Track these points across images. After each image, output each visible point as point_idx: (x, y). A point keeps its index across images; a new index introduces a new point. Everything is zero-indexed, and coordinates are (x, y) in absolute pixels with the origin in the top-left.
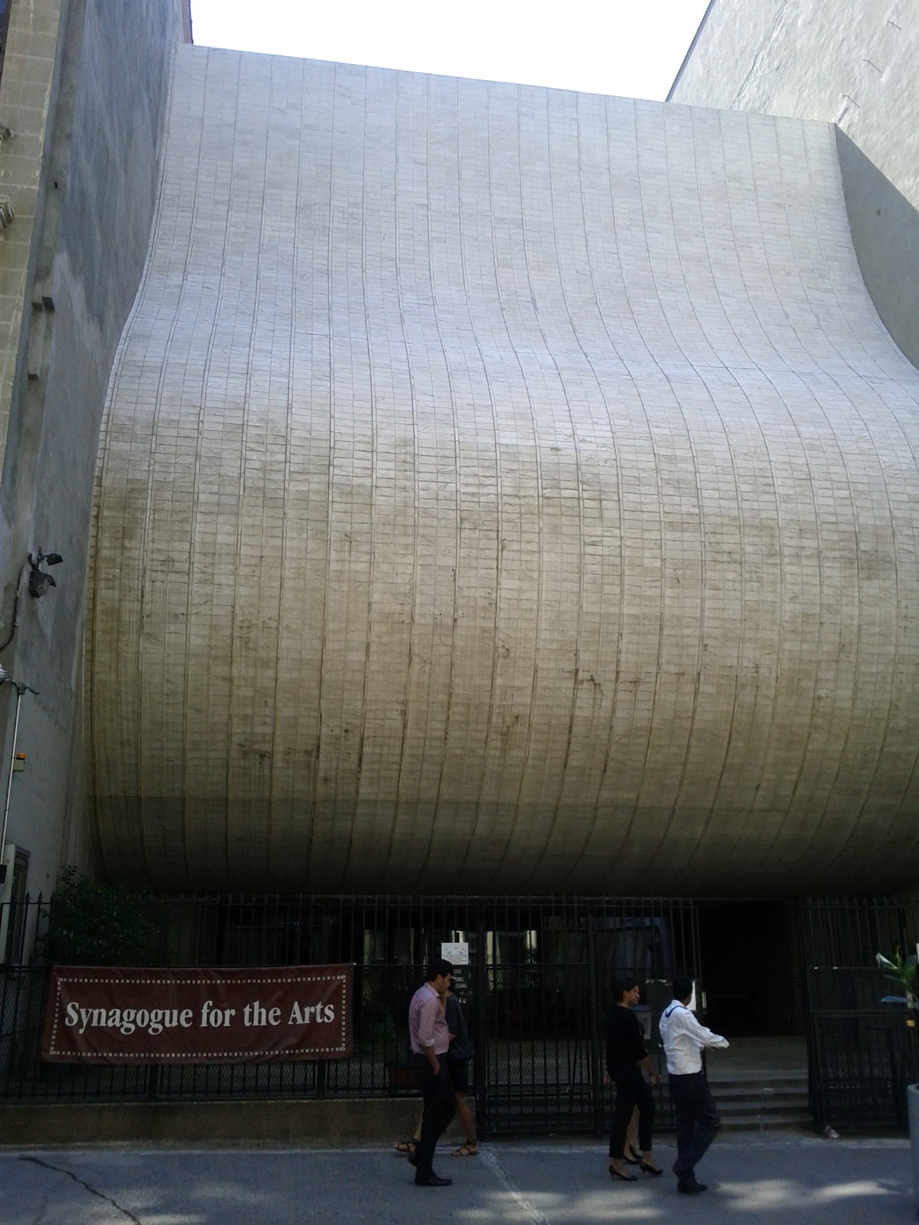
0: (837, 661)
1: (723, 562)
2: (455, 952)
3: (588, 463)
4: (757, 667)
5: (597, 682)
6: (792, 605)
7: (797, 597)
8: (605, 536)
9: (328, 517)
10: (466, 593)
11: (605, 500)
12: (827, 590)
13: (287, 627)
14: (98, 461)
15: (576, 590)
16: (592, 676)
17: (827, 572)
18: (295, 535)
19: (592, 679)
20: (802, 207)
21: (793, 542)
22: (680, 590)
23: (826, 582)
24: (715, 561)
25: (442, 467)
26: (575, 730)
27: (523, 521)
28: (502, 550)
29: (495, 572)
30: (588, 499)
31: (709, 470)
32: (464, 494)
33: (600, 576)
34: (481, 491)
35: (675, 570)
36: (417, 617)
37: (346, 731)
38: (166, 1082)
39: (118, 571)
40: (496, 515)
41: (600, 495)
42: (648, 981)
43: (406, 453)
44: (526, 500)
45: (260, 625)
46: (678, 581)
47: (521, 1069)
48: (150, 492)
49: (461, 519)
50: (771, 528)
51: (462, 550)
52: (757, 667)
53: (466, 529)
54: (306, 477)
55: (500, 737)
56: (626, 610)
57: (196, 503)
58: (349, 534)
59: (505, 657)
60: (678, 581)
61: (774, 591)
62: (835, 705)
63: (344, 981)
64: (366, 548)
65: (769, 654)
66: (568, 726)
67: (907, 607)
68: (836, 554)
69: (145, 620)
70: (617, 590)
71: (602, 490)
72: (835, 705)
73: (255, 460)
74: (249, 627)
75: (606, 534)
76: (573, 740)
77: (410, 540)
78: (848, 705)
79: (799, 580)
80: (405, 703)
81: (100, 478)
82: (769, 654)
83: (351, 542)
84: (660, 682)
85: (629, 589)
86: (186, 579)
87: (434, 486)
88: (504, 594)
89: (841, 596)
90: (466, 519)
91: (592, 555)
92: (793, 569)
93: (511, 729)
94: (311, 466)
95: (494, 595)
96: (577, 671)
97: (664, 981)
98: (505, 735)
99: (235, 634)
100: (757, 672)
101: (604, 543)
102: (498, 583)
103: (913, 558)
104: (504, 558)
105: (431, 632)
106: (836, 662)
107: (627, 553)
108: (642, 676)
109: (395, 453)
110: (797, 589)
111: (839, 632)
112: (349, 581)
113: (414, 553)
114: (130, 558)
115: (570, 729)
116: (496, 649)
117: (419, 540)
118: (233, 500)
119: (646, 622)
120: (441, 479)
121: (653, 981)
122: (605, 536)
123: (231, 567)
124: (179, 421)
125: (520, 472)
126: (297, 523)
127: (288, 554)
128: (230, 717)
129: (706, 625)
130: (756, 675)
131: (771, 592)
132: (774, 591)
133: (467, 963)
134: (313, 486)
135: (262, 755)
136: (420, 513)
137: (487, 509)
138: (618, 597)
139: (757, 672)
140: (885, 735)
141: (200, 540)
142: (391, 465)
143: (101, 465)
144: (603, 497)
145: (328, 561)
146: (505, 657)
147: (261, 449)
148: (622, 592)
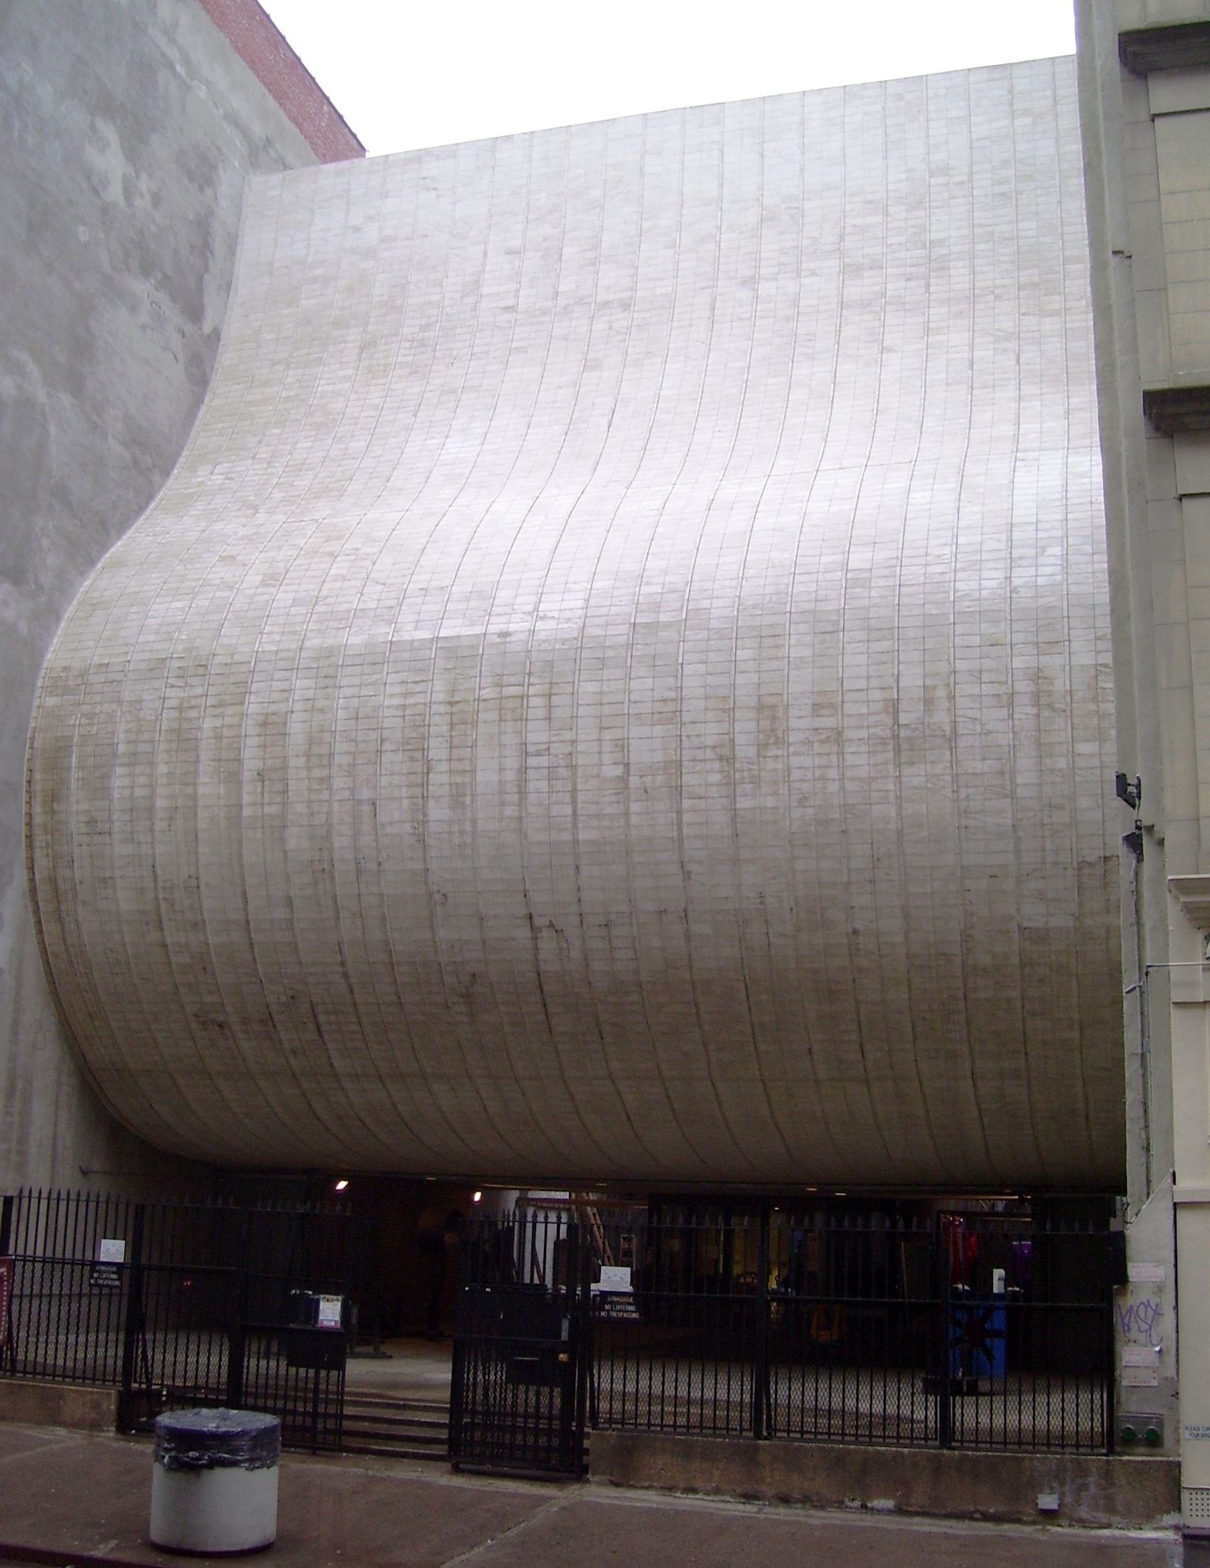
0: (872, 882)
1: (705, 760)
2: (112, 1250)
3: (541, 648)
4: (761, 896)
5: (559, 929)
6: (801, 809)
7: (805, 798)
8: (553, 742)
9: (240, 755)
10: (389, 830)
11: (556, 694)
12: (850, 786)
13: (207, 884)
14: (32, 720)
15: (516, 814)
16: (550, 921)
17: (850, 759)
18: (207, 780)
19: (551, 925)
20: (1039, 192)
21: (804, 723)
22: (649, 802)
23: (849, 774)
24: (694, 760)
25: (367, 677)
26: (546, 988)
27: (454, 733)
28: (428, 773)
29: (420, 801)
30: (535, 696)
31: (699, 636)
32: (388, 707)
33: (546, 795)
34: (407, 702)
35: (641, 777)
36: (337, 864)
37: (293, 997)
38: (109, 1353)
39: (50, 837)
40: (1099, 690)
41: (551, 688)
42: (293, 1292)
43: (328, 666)
44: (460, 706)
45: (182, 885)
46: (646, 791)
47: (163, 1374)
48: (75, 749)
49: (381, 739)
50: (773, 707)
51: (383, 778)
52: (761, 896)
53: (387, 751)
54: (222, 710)
55: (461, 1000)
56: (582, 836)
57: (115, 755)
58: (261, 773)
59: (443, 904)
60: (646, 791)
61: (776, 793)
62: (880, 940)
63: (5, 1274)
64: (278, 787)
65: (774, 878)
66: (537, 984)
67: (967, 797)
68: (863, 734)
69: (78, 886)
70: (569, 810)
71: (554, 681)
72: (880, 940)
73: (174, 696)
74: (172, 888)
75: (553, 739)
76: (548, 1000)
77: (325, 773)
78: (899, 938)
79: (810, 775)
80: (343, 964)
81: (33, 739)
82: (774, 878)
83: (263, 781)
84: (638, 924)
85: (583, 808)
86: (108, 841)
87: (355, 702)
88: (433, 827)
89: (870, 791)
90: (387, 739)
91: (535, 768)
92: (805, 761)
93: (471, 990)
94: (228, 696)
95: (421, 830)
96: (531, 917)
97: (310, 1293)
98: (467, 997)
99: (161, 896)
100: (762, 903)
101: (552, 751)
102: (425, 815)
103: (978, 727)
104: (431, 782)
105: (355, 879)
106: (870, 882)
107: (581, 760)
108: (613, 917)
109: (318, 668)
110: (806, 787)
111: (870, 841)
112: (262, 827)
113: (330, 789)
114: (59, 822)
115: (541, 986)
116: (431, 895)
117: (335, 770)
118: (148, 748)
119: (608, 849)
120: (364, 692)
121: (298, 1292)
122: (553, 742)
123: (148, 823)
124: (108, 664)
125: (458, 671)
126: (209, 766)
127: (200, 803)
128: (176, 987)
129: (686, 847)
130: (763, 906)
131: (770, 795)
132: (776, 793)
133: (122, 1261)
134: (228, 721)
135: (221, 1026)
136: (337, 737)
137: (412, 724)
138: (570, 819)
139: (762, 903)
140: (965, 978)
141: (119, 796)
142: (311, 683)
143: (34, 725)
144: (554, 691)
145: (240, 807)
146: (443, 904)
147: (180, 684)
148: (575, 812)
